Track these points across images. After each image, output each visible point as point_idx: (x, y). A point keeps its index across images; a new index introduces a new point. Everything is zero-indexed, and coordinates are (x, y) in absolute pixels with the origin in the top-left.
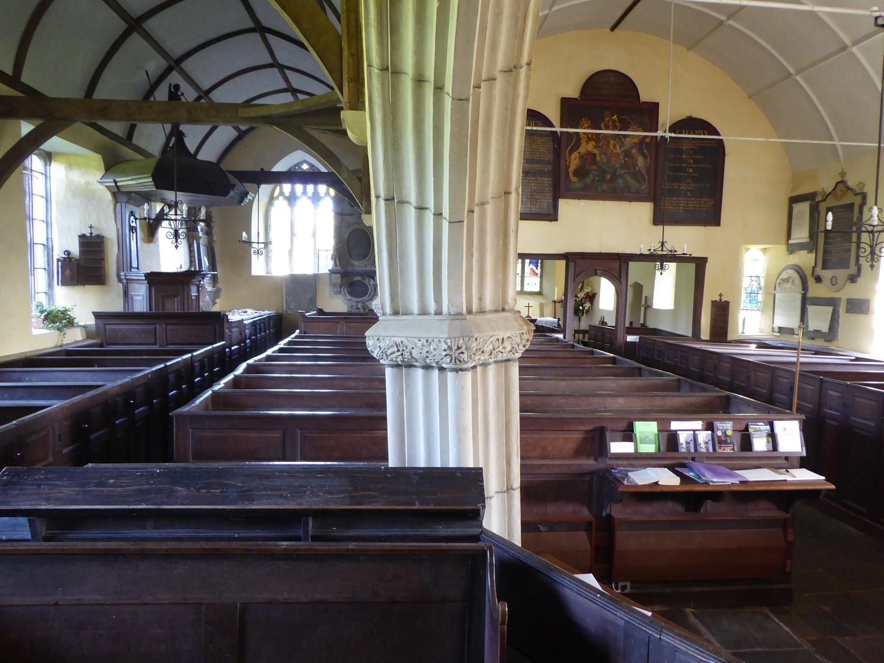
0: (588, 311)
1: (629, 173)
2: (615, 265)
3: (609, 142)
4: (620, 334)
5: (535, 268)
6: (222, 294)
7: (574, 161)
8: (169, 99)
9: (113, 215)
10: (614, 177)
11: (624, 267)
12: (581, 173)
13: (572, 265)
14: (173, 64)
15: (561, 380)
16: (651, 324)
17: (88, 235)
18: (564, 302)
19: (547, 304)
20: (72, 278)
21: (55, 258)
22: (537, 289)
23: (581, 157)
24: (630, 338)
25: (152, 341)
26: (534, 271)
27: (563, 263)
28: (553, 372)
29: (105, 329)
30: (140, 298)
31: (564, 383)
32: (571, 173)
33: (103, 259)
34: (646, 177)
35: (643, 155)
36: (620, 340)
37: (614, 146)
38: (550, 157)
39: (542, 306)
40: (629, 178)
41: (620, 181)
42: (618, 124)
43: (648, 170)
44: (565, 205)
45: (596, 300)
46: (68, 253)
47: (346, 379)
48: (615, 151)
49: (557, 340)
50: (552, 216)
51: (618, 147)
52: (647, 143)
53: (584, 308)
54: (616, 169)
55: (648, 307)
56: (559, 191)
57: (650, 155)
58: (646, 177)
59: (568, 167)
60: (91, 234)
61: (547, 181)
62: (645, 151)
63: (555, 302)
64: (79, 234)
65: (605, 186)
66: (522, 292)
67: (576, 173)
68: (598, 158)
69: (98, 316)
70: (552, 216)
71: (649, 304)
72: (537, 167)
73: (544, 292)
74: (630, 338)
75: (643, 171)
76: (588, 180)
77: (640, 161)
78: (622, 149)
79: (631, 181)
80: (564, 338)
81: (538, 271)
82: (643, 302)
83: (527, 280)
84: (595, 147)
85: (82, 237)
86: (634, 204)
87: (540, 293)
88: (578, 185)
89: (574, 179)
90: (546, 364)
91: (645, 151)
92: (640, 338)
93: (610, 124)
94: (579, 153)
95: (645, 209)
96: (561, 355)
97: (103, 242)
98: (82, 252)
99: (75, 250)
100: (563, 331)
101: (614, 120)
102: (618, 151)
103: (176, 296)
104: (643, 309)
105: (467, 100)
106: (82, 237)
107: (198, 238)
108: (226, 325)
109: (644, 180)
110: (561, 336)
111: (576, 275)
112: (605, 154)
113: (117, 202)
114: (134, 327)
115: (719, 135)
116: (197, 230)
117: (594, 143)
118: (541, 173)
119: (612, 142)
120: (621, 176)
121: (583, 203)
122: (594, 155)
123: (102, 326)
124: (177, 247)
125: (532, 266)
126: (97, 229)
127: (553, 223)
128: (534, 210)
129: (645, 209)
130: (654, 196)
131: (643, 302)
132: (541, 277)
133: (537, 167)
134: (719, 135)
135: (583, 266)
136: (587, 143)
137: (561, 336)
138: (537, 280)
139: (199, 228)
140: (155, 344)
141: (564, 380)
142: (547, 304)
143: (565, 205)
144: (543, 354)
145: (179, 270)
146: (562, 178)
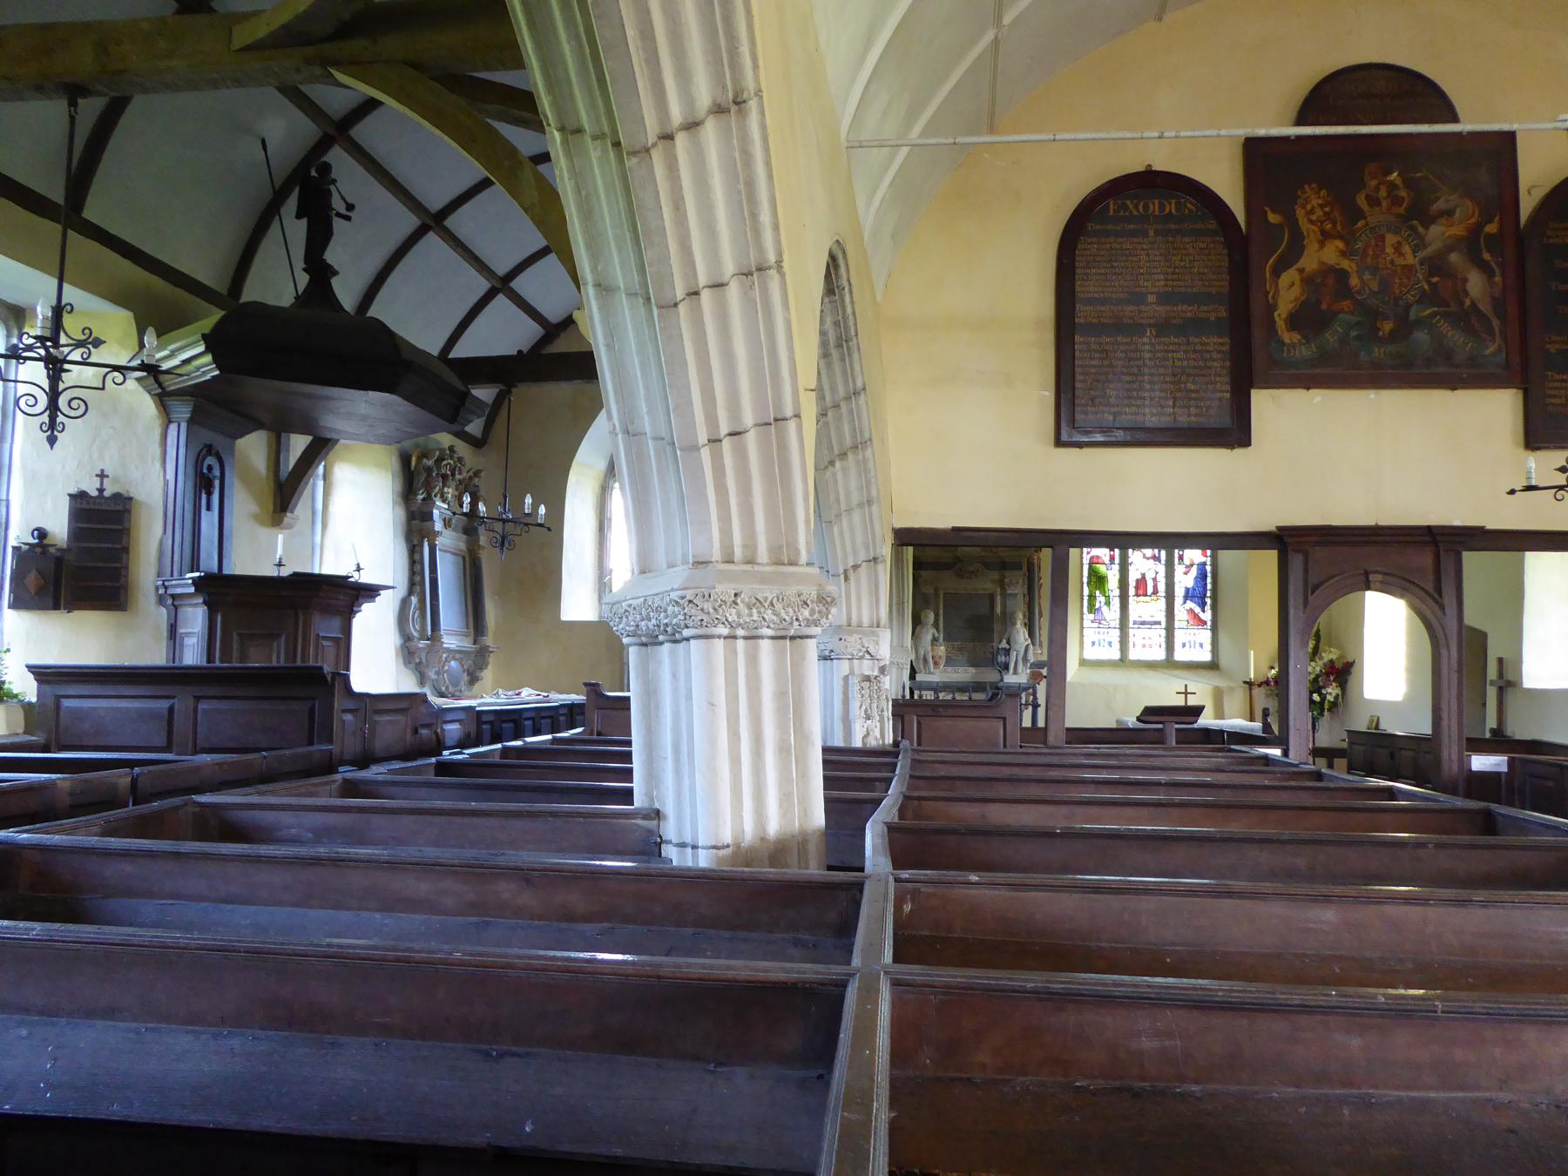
0: (1334, 705)
1: (1445, 315)
2: (1428, 560)
3: (1383, 238)
4: (1450, 751)
5: (1197, 610)
6: (491, 659)
7: (1287, 292)
8: (1068, 730)
9: (158, 451)
10: (1405, 327)
11: (1447, 564)
12: (1308, 319)
13: (1296, 562)
14: (331, 131)
15: (1315, 899)
16: (1521, 729)
17: (94, 493)
18: (1278, 686)
19: (1232, 689)
20: (41, 591)
21: (12, 542)
22: (1206, 656)
23: (1308, 281)
24: (1481, 762)
25: (161, 741)
26: (1196, 616)
27: (1271, 556)
28: (1265, 857)
29: (58, 707)
30: (194, 640)
31: (1328, 915)
32: (1280, 324)
33: (126, 550)
34: (1496, 323)
35: (1484, 267)
36: (1450, 766)
37: (1398, 248)
38: (1222, 285)
39: (1218, 695)
40: (1445, 327)
41: (1421, 337)
42: (1403, 193)
43: (1499, 305)
44: (1263, 402)
45: (1352, 680)
46: (42, 534)
47: (392, 865)
48: (1400, 261)
49: (1266, 760)
50: (1234, 432)
51: (1407, 249)
52: (1489, 237)
53: (1323, 698)
54: (1408, 306)
55: (1508, 683)
56: (1250, 368)
57: (1502, 266)
58: (1496, 323)
59: (1272, 308)
60: (101, 490)
61: (1216, 345)
62: (1487, 256)
63: (1250, 684)
64: (73, 491)
65: (1378, 352)
66: (1169, 664)
67: (1294, 321)
68: (1354, 281)
69: (43, 674)
70: (1234, 432)
71: (1509, 676)
72: (1188, 311)
73: (1224, 660)
74: (1481, 762)
75: (1485, 307)
76: (1330, 338)
77: (1475, 284)
78: (1422, 254)
79: (1454, 337)
80: (1286, 754)
81: (1207, 616)
82: (1492, 672)
83: (1180, 636)
84: (1343, 254)
85: (79, 498)
86: (1462, 395)
87: (1213, 666)
88: (1304, 352)
89: (1288, 337)
90: (1236, 827)
91: (1487, 256)
92: (1511, 762)
93: (1383, 193)
94: (1301, 271)
95: (1499, 408)
96: (1285, 798)
97: (128, 511)
98: (76, 533)
99: (59, 527)
100: (1282, 741)
101: (1392, 186)
102: (1410, 260)
103: (276, 637)
104: (1492, 693)
105: (992, 130)
106: (79, 498)
107: (432, 535)
108: (339, 703)
109: (1491, 331)
110: (1276, 752)
111: (1310, 589)
112: (1374, 270)
113: (170, 422)
114: (123, 704)
115: (1455, 119)
116: (430, 517)
117: (1340, 244)
118: (1196, 326)
119: (1391, 239)
120: (1419, 323)
121: (1318, 398)
122: (1342, 275)
123: (50, 702)
124: (52, 441)
125: (1190, 604)
126: (116, 480)
127: (1239, 452)
128: (1184, 420)
129: (1499, 408)
130: (1516, 370)
131: (1492, 672)
132: (1214, 629)
133: (1188, 311)
134: (1455, 119)
135: (1321, 563)
136: (1322, 244)
137: (1276, 752)
138: (1205, 635)
139: (436, 512)
140: (168, 748)
141: (1327, 899)
142: (1232, 689)
143: (1263, 402)
144: (1226, 796)
145: (271, 572)
146: (1258, 333)
